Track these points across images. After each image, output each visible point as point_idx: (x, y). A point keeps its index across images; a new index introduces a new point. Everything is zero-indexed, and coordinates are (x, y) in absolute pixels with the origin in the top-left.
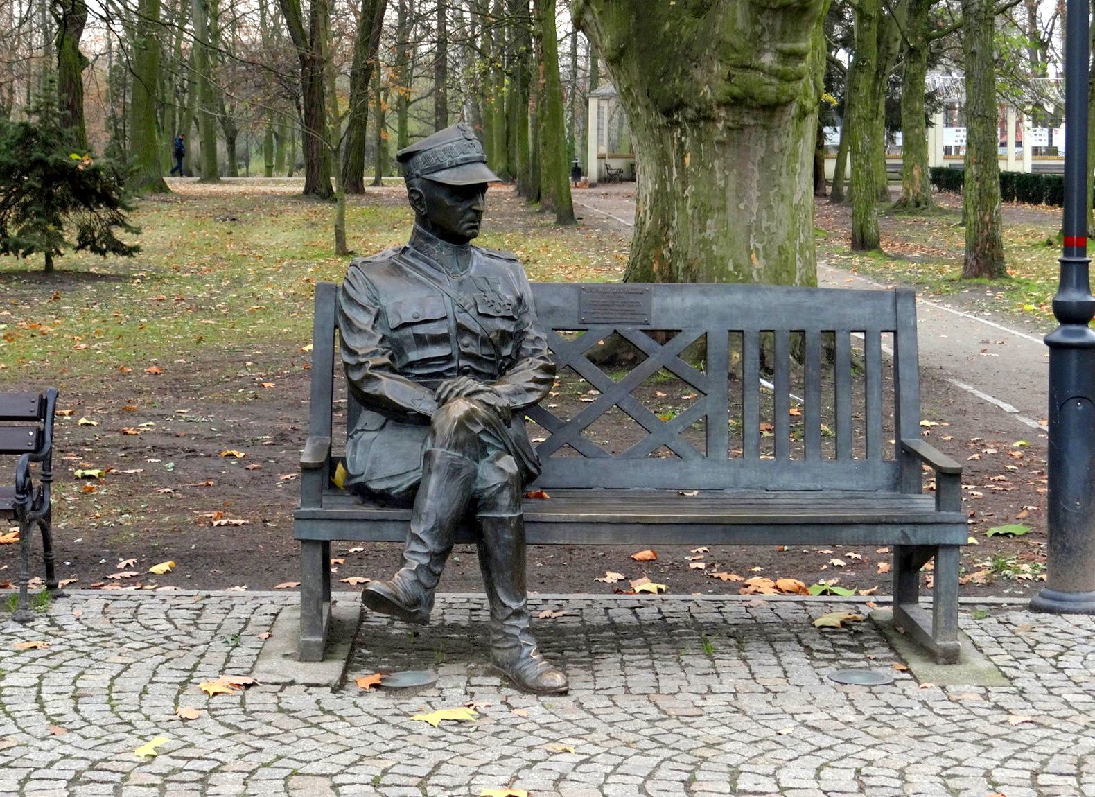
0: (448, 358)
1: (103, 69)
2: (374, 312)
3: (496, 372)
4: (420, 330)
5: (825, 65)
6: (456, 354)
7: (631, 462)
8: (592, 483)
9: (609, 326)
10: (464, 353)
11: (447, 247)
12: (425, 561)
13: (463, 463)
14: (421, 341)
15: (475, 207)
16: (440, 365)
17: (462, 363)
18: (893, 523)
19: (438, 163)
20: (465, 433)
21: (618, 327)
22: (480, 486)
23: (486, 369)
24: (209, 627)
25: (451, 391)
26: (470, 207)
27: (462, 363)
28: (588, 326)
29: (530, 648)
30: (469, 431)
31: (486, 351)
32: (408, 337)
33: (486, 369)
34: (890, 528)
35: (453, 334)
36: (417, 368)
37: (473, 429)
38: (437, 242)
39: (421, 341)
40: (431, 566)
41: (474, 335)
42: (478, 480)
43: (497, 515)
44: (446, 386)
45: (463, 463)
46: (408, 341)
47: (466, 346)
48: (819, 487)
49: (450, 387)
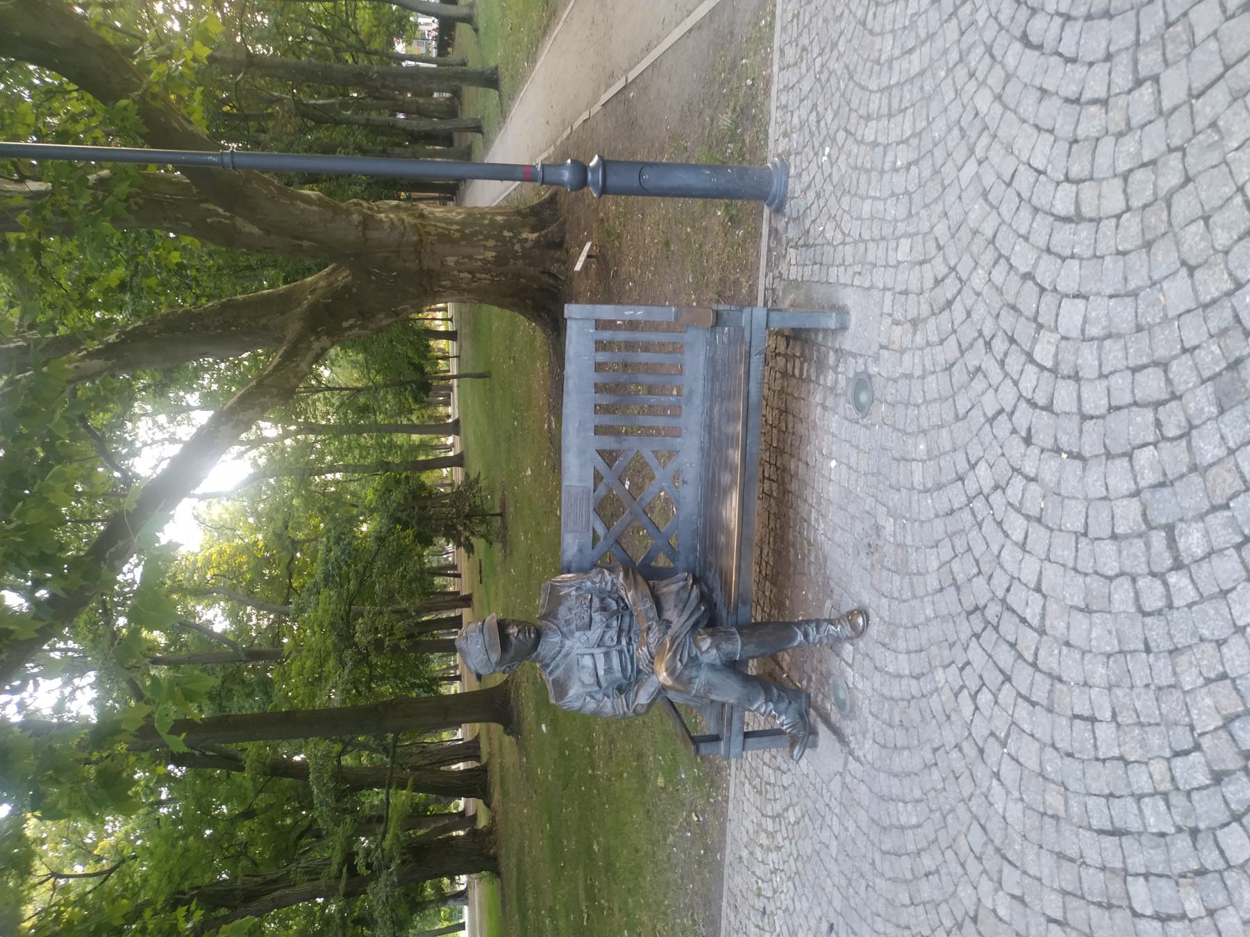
0: (620, 652)
2: (588, 699)
14: (609, 670)
17: (624, 642)
22: (718, 662)
27: (624, 642)
35: (603, 649)
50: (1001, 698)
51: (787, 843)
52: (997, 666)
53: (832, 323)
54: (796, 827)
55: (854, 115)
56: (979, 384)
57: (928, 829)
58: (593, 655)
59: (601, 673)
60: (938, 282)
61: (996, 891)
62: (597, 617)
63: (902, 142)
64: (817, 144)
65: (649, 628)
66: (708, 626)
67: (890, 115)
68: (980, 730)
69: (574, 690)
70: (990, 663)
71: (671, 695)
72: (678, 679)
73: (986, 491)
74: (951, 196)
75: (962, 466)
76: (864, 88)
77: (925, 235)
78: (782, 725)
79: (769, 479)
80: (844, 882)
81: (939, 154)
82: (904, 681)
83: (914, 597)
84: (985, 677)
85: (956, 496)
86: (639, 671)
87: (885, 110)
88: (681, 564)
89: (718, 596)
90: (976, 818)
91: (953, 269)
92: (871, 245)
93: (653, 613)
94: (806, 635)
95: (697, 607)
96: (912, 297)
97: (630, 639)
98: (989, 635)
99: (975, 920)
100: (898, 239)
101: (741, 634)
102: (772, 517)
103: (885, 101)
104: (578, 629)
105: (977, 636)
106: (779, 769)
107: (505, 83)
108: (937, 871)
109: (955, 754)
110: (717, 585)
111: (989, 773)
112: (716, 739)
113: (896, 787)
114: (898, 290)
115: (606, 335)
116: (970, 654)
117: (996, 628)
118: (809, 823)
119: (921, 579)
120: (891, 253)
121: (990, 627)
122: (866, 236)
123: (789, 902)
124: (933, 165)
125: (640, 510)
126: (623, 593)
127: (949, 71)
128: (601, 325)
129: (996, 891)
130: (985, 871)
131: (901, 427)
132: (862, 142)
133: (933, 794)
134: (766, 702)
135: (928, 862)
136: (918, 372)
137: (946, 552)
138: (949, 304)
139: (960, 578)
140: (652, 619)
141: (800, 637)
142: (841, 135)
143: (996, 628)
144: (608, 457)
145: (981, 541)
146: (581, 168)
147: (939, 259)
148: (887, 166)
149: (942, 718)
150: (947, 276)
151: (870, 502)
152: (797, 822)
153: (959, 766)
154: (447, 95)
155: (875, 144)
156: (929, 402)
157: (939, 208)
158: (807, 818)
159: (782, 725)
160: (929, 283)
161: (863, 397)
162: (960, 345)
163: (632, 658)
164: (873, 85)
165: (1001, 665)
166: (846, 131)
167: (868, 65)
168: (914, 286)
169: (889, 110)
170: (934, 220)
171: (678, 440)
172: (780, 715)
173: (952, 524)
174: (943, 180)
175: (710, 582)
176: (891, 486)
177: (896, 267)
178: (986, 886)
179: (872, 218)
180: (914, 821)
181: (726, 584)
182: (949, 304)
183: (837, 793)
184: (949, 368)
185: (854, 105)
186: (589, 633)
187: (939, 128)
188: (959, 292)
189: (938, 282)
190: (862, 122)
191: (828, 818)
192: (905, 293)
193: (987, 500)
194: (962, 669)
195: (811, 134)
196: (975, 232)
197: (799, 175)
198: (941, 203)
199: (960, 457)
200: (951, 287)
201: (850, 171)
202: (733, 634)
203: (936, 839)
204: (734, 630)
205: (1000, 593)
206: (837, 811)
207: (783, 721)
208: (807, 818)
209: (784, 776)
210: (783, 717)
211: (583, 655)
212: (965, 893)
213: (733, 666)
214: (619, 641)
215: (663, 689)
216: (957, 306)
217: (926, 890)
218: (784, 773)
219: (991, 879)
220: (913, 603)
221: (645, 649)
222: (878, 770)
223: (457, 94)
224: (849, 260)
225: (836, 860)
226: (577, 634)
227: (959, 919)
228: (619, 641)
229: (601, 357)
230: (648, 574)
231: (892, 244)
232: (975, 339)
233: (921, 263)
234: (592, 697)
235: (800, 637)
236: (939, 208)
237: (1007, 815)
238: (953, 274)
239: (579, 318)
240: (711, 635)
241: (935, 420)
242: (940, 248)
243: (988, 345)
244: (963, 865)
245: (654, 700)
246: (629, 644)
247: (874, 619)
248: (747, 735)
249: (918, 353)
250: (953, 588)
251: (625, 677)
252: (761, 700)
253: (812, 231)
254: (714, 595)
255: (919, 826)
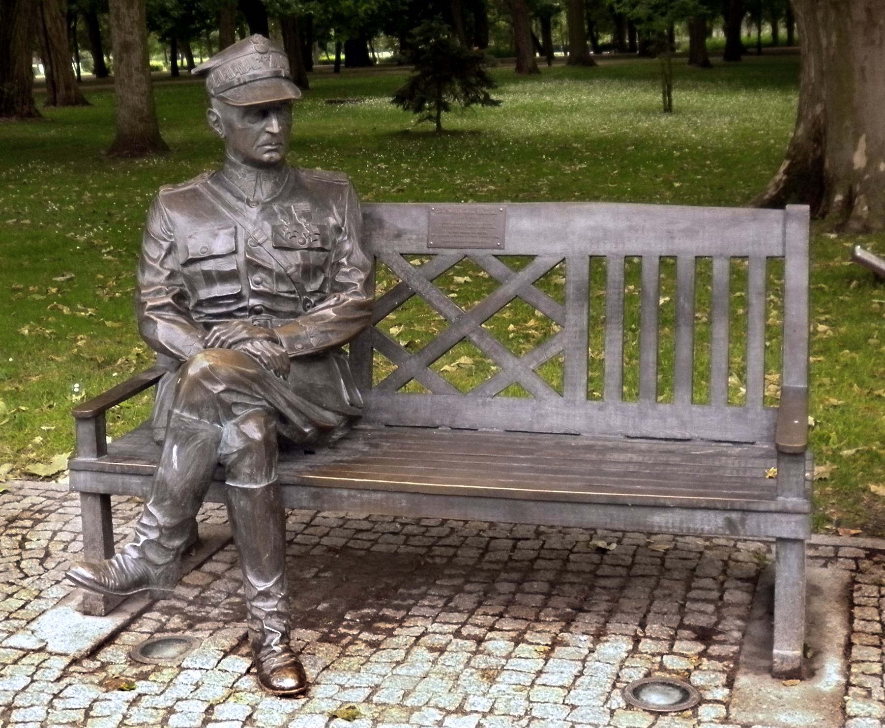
0: (238, 297)
2: (165, 245)
3: (300, 309)
4: (208, 266)
6: (245, 292)
7: (480, 401)
8: (438, 422)
9: (459, 251)
10: (254, 291)
11: (249, 172)
12: (154, 535)
13: (201, 426)
14: (210, 278)
15: (268, 129)
16: (229, 305)
17: (253, 302)
18: (716, 509)
19: (228, 81)
20: (202, 393)
22: (225, 451)
23: (287, 308)
25: (218, 338)
26: (263, 129)
27: (253, 302)
28: (437, 251)
29: (273, 635)
30: (208, 391)
31: (283, 288)
32: (196, 273)
33: (287, 308)
34: (712, 514)
35: (243, 268)
36: (206, 307)
37: (210, 386)
38: (239, 167)
39: (210, 278)
40: (162, 541)
41: (269, 271)
42: (222, 444)
43: (240, 486)
44: (215, 332)
45: (201, 426)
46: (198, 277)
47: (258, 283)
48: (687, 436)
49: (218, 334)
58: (235, 252)
62: (295, 258)
65: (275, 341)
66: (280, 437)
69: (180, 219)
71: (169, 380)
72: (196, 383)
78: (123, 552)
79: (514, 547)
86: (208, 327)
89: (323, 457)
95: (310, 422)
97: (258, 313)
101: (267, 488)
102: (451, 551)
104: (276, 230)
106: (48, 554)
110: (342, 455)
112: (101, 449)
115: (757, 277)
126: (332, 302)
134: (159, 528)
140: (291, 348)
141: (261, 586)
144: (546, 280)
161: (655, 698)
163: (229, 315)
171: (582, 394)
172: (141, 550)
175: (348, 444)
181: (340, 468)
186: (269, 245)
204: (274, 478)
207: (127, 556)
209: (36, 562)
210: (135, 554)
211: (235, 235)
213: (215, 475)
214: (256, 294)
221: (244, 334)
222: (51, 705)
228: (256, 294)
229: (720, 270)
230: (360, 342)
234: (169, 251)
235: (261, 586)
239: (784, 233)
240: (266, 440)
245: (163, 350)
246: (253, 311)
247: (289, 705)
248: (105, 499)
252: (161, 519)
254: (326, 451)
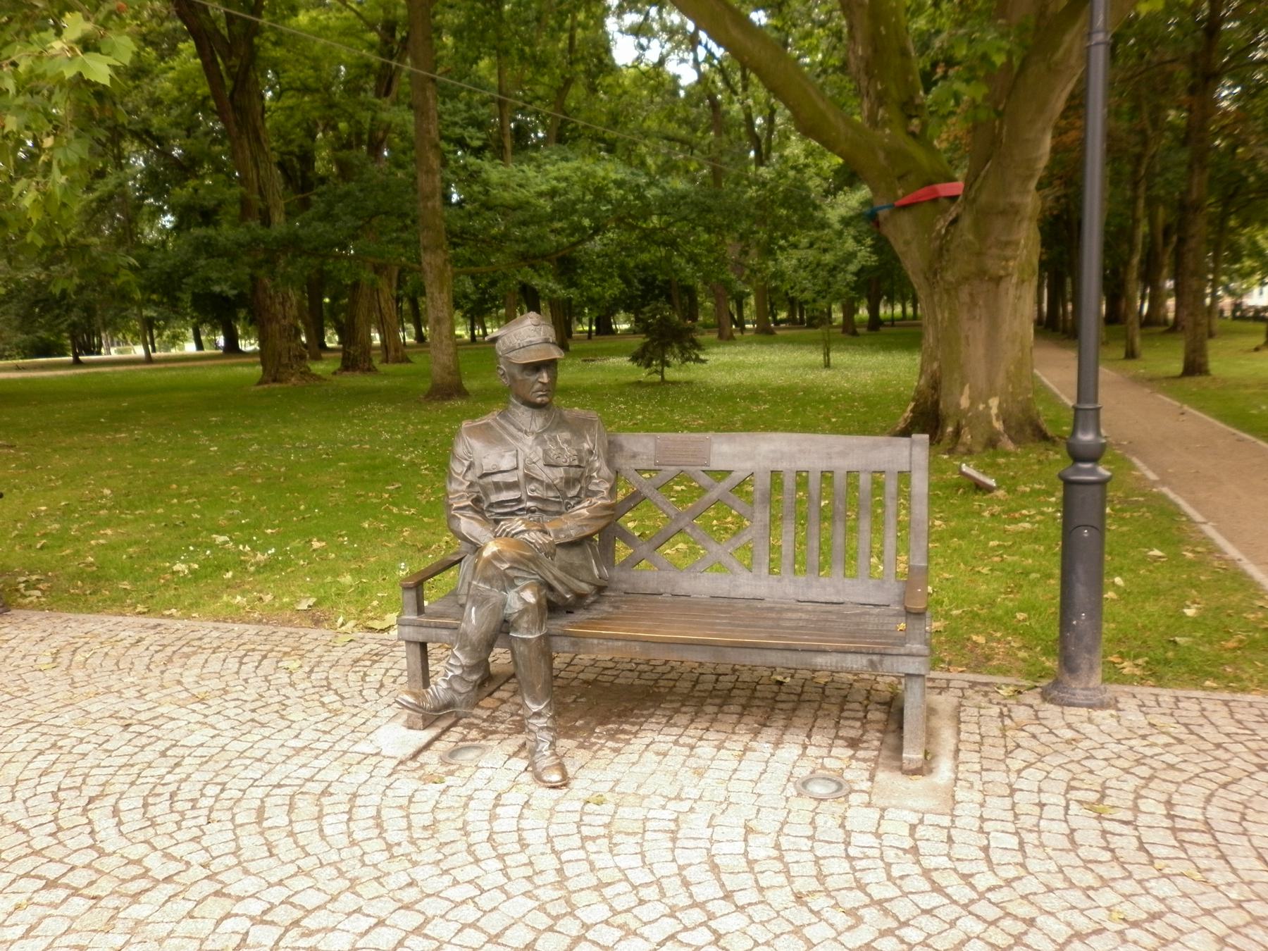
0: (519, 501)
1: (1165, 271)
2: (467, 463)
3: (563, 509)
4: (497, 478)
5: (424, 264)
6: (524, 497)
12: (458, 672)
14: (498, 487)
17: (529, 504)
21: (684, 468)
22: (509, 611)
24: (145, 780)
27: (529, 504)
34: (859, 656)
39: (498, 487)
41: (541, 482)
50: (469, 932)
51: (300, 693)
52: (506, 929)
53: (912, 755)
54: (317, 703)
55: (1173, 787)
56: (841, 920)
57: (316, 845)
58: (516, 468)
59: (497, 478)
60: (966, 877)
61: (252, 918)
62: (559, 473)
63: (1141, 843)
64: (1132, 743)
65: (545, 532)
66: (549, 601)
67: (1174, 830)
68: (432, 907)
69: (477, 445)
70: (508, 922)
71: (469, 560)
73: (712, 924)
74: (1075, 897)
75: (741, 898)
76: (1208, 800)
77: (1023, 865)
78: (436, 684)
79: (717, 680)
80: (258, 754)
81: (1129, 887)
82: (486, 826)
83: (584, 839)
84: (495, 915)
85: (707, 890)
86: (497, 522)
87: (1180, 824)
88: (616, 574)
89: (580, 616)
90: (334, 899)
91: (982, 896)
92: (1007, 802)
93: (563, 538)
94: (538, 715)
95: (570, 590)
96: (944, 848)
97: (533, 512)
98: (542, 921)
99: (217, 894)
100: (1017, 833)
101: (540, 638)
102: (672, 683)
103: (1194, 825)
104: (545, 452)
105: (542, 908)
107: (1192, 383)
108: (271, 855)
109: (404, 879)
111: (383, 915)
112: (420, 610)
113: (364, 813)
114: (953, 832)
115: (891, 486)
116: (522, 900)
117: (550, 929)
118: (322, 718)
119: (605, 848)
120: (999, 826)
121: (550, 922)
122: (1018, 796)
123: (235, 696)
124: (1114, 879)
125: (682, 524)
126: (586, 504)
127: (1239, 905)
128: (904, 477)
129: (252, 918)
130: (272, 906)
131: (785, 830)
132: (1139, 796)
133: (359, 852)
135: (285, 847)
136: (853, 851)
137: (639, 876)
138: (937, 889)
139: (608, 892)
140: (557, 537)
141: (535, 708)
142: (1144, 771)
143: (550, 929)
145: (654, 916)
146: (1094, 455)
147: (994, 881)
148: (1108, 826)
149: (444, 866)
150: (973, 887)
151: (695, 793)
152: (323, 704)
153: (391, 882)
154: (1171, 315)
155: (1136, 809)
156: (816, 863)
157: (1058, 882)
158: (327, 715)
159: (436, 684)
160: (965, 868)
162: (887, 900)
163: (513, 513)
164: (1213, 812)
165: (508, 932)
166: (1151, 778)
167: (1240, 807)
168: (958, 851)
169: (1182, 830)
170: (1044, 878)
173: (673, 885)
174: (1096, 889)
175: (597, 606)
176: (713, 816)
177: (981, 830)
178: (255, 908)
179: (1042, 805)
180: (328, 831)
182: (937, 889)
183: (357, 748)
184: (862, 887)
185: (1185, 788)
186: (541, 463)
187: (1162, 888)
188: (955, 902)
189: (966, 877)
190: (1164, 797)
191: (328, 737)
192: (950, 840)
193: (701, 925)
194: (501, 888)
195: (1144, 737)
196: (1031, 922)
197: (1090, 721)
198: (1066, 885)
199: (753, 896)
200: (962, 893)
201: (1100, 781)
202: (540, 629)
203: (308, 855)
204: (544, 631)
205: (590, 935)
206: (337, 747)
207: (439, 686)
208: (327, 715)
210: (444, 685)
212: (249, 885)
213: (503, 629)
214: (531, 499)
215: (477, 548)
216: (937, 900)
217: (251, 843)
218: (378, 690)
219: (264, 913)
220: (577, 837)
221: (523, 527)
223: (1174, 328)
224: (987, 776)
225: (283, 745)
226: (540, 450)
227: (219, 877)
228: (531, 499)
230: (604, 536)
231: (1011, 827)
232: (897, 919)
233: (988, 860)
234: (469, 468)
235: (535, 708)
236: (1058, 882)
237: (337, 933)
238: (975, 896)
239: (912, 453)
240: (539, 603)
241: (795, 869)
242: (1008, 882)
243: (888, 932)
244: (280, 883)
245: (465, 539)
246: (529, 510)
248: (423, 646)
249: (876, 853)
250: (595, 882)
251: (491, 505)
252: (464, 660)
253: (1023, 734)
254: (582, 611)
255: (323, 837)
